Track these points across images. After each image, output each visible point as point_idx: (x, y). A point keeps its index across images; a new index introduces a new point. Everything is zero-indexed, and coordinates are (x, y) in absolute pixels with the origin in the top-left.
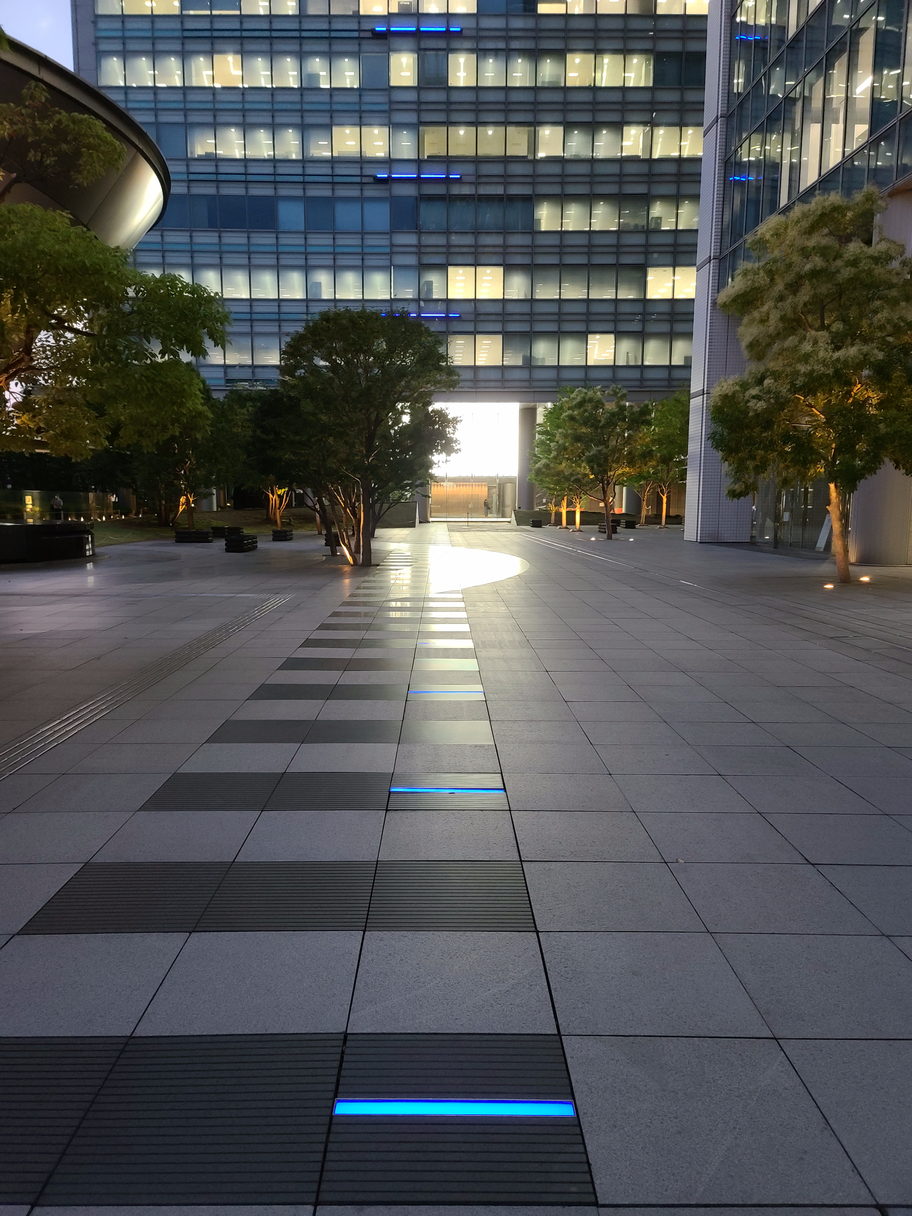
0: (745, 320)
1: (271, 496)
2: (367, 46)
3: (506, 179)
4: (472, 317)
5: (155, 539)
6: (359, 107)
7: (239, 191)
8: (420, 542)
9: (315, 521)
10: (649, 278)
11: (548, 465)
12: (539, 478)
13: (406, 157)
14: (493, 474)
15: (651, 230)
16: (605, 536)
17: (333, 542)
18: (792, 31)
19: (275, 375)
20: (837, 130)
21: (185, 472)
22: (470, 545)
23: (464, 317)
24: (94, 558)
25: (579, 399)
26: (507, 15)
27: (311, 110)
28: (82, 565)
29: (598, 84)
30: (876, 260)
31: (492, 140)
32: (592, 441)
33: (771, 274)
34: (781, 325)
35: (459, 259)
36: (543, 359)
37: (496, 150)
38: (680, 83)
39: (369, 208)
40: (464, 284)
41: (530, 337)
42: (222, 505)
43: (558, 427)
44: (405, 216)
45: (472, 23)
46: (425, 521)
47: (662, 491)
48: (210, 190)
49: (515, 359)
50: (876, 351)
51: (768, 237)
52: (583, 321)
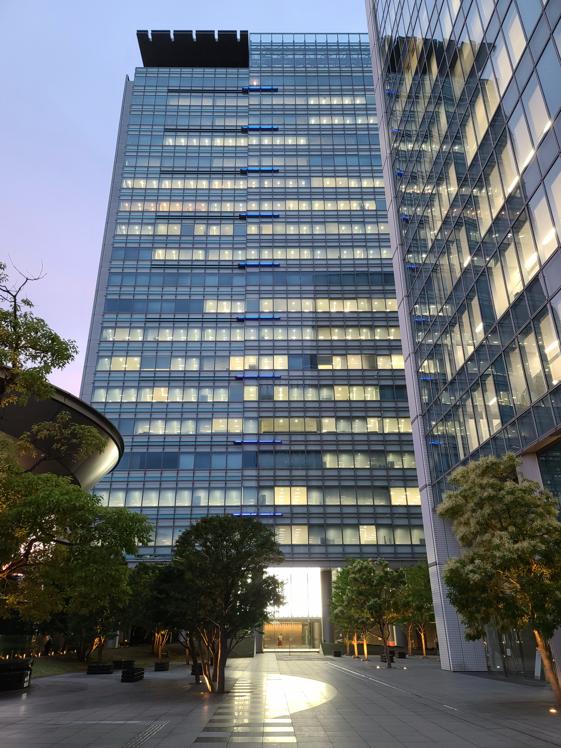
0: (455, 522)
1: (157, 635)
2: (233, 384)
3: (306, 443)
4: (289, 515)
5: (72, 672)
6: (227, 411)
7: (160, 450)
8: (256, 671)
9: (186, 654)
10: (391, 493)
11: (343, 611)
12: (337, 620)
13: (251, 432)
14: (305, 616)
15: (389, 468)
16: (386, 664)
17: (197, 671)
18: (450, 378)
19: (168, 551)
20: (483, 423)
21: (102, 620)
22: (293, 673)
23: (285, 515)
24: (28, 690)
25: (358, 567)
26: (303, 370)
27: (202, 412)
28: (19, 696)
29: (351, 399)
30: (525, 491)
31: (297, 425)
32: (370, 594)
33: (465, 498)
34: (478, 527)
35: (280, 483)
36: (333, 540)
37: (300, 429)
38: (394, 398)
39: (230, 457)
40: (282, 497)
41: (324, 527)
42: (122, 642)
43: (347, 584)
44: (252, 460)
45: (286, 373)
46: (260, 652)
47: (420, 629)
48: (144, 450)
49: (316, 540)
50: (540, 544)
51: (458, 477)
52: (355, 518)
